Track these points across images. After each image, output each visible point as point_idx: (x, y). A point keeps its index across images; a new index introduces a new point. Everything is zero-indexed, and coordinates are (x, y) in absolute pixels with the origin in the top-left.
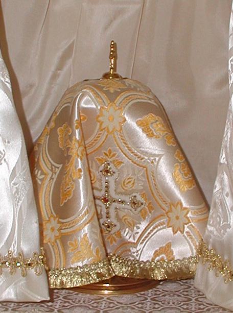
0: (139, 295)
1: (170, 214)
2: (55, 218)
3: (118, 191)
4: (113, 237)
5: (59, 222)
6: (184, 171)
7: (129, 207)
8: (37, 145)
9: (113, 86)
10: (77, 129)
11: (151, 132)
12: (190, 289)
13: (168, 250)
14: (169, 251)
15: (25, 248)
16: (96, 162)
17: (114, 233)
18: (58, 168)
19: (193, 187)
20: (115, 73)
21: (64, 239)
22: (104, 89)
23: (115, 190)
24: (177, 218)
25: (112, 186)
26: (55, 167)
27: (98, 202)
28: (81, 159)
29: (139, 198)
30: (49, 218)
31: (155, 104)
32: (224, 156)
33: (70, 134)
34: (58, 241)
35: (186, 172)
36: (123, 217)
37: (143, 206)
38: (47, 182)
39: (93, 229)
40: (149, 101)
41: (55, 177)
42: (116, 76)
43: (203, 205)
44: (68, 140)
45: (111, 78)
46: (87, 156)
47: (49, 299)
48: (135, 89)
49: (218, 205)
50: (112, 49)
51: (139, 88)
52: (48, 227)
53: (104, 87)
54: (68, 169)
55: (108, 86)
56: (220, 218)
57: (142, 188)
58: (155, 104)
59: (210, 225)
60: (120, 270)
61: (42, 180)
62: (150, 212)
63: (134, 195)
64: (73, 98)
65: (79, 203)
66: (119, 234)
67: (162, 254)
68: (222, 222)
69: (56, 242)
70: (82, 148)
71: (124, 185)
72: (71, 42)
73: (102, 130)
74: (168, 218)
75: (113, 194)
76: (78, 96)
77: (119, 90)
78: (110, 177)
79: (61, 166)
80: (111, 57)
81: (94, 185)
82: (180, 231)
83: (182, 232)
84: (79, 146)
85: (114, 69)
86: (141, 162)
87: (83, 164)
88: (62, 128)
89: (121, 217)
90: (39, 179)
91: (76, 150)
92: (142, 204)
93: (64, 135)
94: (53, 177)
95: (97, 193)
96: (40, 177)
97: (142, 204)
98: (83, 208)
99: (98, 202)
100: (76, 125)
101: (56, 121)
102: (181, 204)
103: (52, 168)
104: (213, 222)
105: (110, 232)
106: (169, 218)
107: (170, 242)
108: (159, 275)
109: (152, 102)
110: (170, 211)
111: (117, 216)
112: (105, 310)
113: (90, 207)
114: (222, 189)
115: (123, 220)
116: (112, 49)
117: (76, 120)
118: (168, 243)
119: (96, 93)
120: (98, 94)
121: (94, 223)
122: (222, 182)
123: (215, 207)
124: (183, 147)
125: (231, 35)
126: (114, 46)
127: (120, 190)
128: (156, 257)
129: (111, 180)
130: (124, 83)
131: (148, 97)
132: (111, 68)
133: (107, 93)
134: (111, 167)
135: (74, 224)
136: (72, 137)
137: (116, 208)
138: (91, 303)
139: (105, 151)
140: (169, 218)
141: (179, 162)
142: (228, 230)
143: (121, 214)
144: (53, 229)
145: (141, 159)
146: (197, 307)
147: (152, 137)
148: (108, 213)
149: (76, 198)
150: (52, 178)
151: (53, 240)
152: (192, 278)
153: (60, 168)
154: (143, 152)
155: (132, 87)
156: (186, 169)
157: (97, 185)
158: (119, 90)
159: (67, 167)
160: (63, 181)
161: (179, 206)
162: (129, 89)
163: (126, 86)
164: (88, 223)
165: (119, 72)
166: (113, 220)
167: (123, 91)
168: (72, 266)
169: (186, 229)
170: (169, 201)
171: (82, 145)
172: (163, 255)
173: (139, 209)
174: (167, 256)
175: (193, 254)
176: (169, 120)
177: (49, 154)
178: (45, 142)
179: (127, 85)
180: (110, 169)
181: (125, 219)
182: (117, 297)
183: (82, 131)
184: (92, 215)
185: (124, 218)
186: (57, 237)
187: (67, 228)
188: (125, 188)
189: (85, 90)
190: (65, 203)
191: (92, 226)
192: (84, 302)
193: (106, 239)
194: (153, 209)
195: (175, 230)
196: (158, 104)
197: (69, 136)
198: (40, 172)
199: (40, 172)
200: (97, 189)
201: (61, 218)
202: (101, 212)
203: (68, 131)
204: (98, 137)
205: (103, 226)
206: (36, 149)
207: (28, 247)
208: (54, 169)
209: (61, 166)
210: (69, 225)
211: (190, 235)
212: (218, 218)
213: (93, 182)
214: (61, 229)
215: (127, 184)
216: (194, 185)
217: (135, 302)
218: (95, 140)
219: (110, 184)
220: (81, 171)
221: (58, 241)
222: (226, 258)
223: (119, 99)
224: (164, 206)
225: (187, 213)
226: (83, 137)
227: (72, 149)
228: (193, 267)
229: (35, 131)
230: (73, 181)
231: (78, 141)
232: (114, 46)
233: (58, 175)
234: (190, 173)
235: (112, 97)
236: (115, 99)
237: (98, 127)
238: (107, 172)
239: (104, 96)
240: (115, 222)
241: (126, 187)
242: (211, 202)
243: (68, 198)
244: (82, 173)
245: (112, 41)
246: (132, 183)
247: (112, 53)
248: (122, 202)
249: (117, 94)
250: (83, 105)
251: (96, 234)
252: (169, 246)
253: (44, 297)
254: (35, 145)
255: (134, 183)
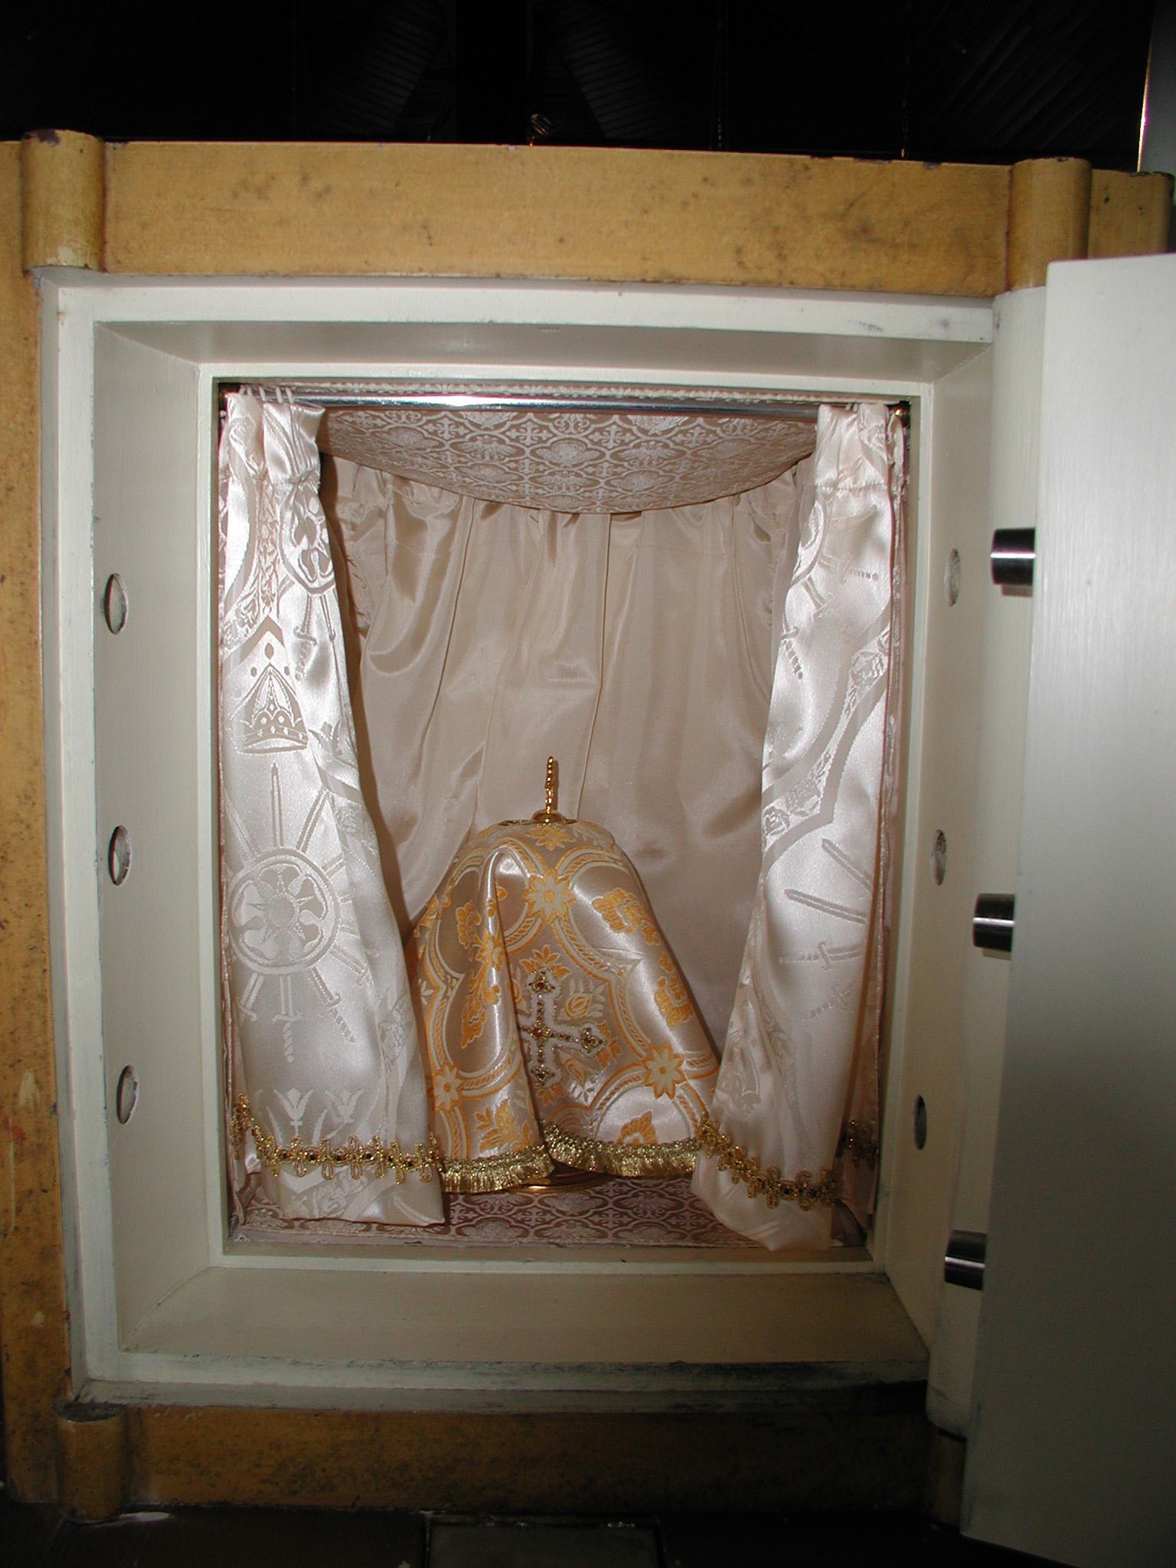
0: (593, 1194)
1: (650, 1064)
2: (452, 1068)
3: (559, 1018)
4: (549, 1092)
5: (458, 1076)
6: (674, 990)
7: (579, 1047)
8: (418, 928)
9: (554, 835)
10: (491, 915)
11: (617, 921)
12: (443, 449)
13: (646, 1126)
14: (648, 1128)
15: (405, 1137)
16: (521, 968)
17: (552, 1086)
18: (457, 979)
19: (690, 1016)
20: (554, 812)
21: (467, 1106)
22: (537, 844)
23: (555, 1020)
24: (663, 1071)
25: (550, 1009)
26: (453, 977)
27: (524, 1034)
28: (498, 969)
29: (596, 1032)
30: (441, 1066)
31: (622, 869)
32: (748, 973)
33: (478, 924)
34: (456, 1108)
35: (678, 991)
36: (567, 1061)
37: (602, 1046)
38: (437, 1003)
39: (518, 1092)
40: (614, 865)
41: (452, 994)
42: (556, 818)
43: (708, 1050)
44: (476, 935)
45: (547, 821)
46: (508, 961)
47: (443, 1221)
48: (589, 843)
49: (737, 1058)
50: (550, 772)
51: (597, 839)
52: (440, 1081)
53: (536, 840)
54: (476, 986)
55: (542, 838)
56: (740, 1082)
57: (601, 1014)
58: (622, 869)
59: (722, 1090)
60: (565, 1153)
61: (430, 998)
62: (615, 1056)
63: (587, 1026)
64: (484, 859)
65: (493, 1052)
66: (560, 1088)
67: (635, 1131)
68: (744, 1089)
69: (454, 1111)
70: (499, 949)
71: (570, 1008)
72: (477, 750)
73: (533, 915)
74: (645, 1071)
75: (551, 1026)
76: (491, 857)
77: (563, 847)
78: (546, 995)
79: (462, 977)
80: (549, 785)
81: (518, 1007)
82: (667, 1093)
83: (671, 1096)
84: (495, 947)
85: (554, 805)
86: (600, 973)
87: (501, 979)
88: (464, 909)
89: (563, 1062)
90: (425, 997)
91: (490, 953)
92: (601, 1042)
93: (467, 923)
94: (449, 994)
95: (524, 1021)
96: (425, 992)
97: (601, 1042)
98: (500, 1057)
99: (524, 1034)
100: (488, 908)
101: (451, 895)
102: (670, 1048)
103: (447, 979)
104: (727, 1085)
105: (543, 1085)
106: (648, 1069)
107: (650, 1113)
108: (629, 1167)
109: (620, 867)
110: (650, 1058)
111: (557, 1060)
112: (537, 1228)
113: (512, 1053)
114: (746, 1031)
115: (567, 1066)
116: (550, 772)
117: (490, 901)
118: (647, 1113)
119: (522, 853)
120: (527, 853)
121: (520, 1081)
122: (744, 1017)
123: (731, 1058)
124: (663, 928)
125: (767, 766)
126: (553, 767)
127: (563, 1016)
128: (624, 1136)
129: (548, 999)
130: (570, 833)
131: (612, 858)
132: (548, 805)
133: (542, 851)
134: (549, 979)
135: (485, 1083)
136: (483, 929)
137: (556, 1047)
138: (513, 1212)
139: (537, 951)
140: (648, 1069)
141: (665, 975)
142: (755, 1105)
143: (564, 1056)
144: (447, 1088)
145: (601, 967)
146: (443, 457)
147: (620, 929)
148: (541, 1055)
149: (488, 1038)
150: (445, 996)
151: (448, 1107)
152: (689, 1175)
153: (461, 980)
154: (604, 954)
155: (585, 839)
156: (677, 986)
157: (522, 1006)
158: (563, 847)
159: (472, 982)
160: (467, 1005)
161: (666, 1051)
162: (579, 844)
163: (574, 837)
164: (509, 1081)
165: (561, 810)
166: (549, 1065)
167: (570, 847)
168: (482, 1156)
169: (679, 1092)
170: (649, 1042)
171: (500, 945)
172: (637, 1135)
173: (595, 1051)
174: (645, 1136)
175: (689, 1133)
176: (645, 891)
177: (442, 954)
178: (430, 921)
179: (576, 835)
180: (546, 982)
181: (570, 1066)
182: (556, 1198)
183: (500, 919)
184: (517, 1066)
185: (570, 1063)
186: (456, 1102)
187: (473, 1089)
188: (572, 1015)
189: (504, 846)
190: (469, 1044)
191: (517, 1086)
192: (500, 1209)
193: (537, 1095)
194: (618, 1052)
195: (659, 1092)
196: (629, 871)
197: (477, 927)
198: (425, 983)
199: (425, 983)
200: (523, 1013)
201: (463, 1070)
202: (529, 1052)
203: (477, 919)
204: (526, 927)
205: (532, 1075)
206: (417, 933)
207: (413, 1135)
208: (449, 981)
209: (462, 977)
210: (477, 1084)
211: (685, 1103)
212: (737, 1082)
213: (517, 1001)
214: (463, 1089)
215: (575, 1007)
216: (691, 1014)
217: (588, 1211)
218: (521, 932)
219: (545, 1015)
220: (498, 991)
221: (456, 1108)
222: (751, 1154)
223: (564, 862)
224: (639, 1049)
225: (680, 1064)
226: (501, 927)
227: (482, 951)
228: (691, 1159)
229: (414, 895)
230: (484, 1007)
231: (493, 937)
232: (553, 767)
233: (457, 992)
234: (685, 992)
235: (550, 859)
236: (556, 862)
237: (526, 909)
238: (541, 986)
239: (536, 858)
240: (552, 1068)
241: (573, 1012)
242: (723, 1050)
243: (475, 1036)
244: (499, 994)
245: (551, 758)
246: (585, 1004)
247: (549, 779)
248: (568, 1038)
249: (560, 852)
250: (502, 870)
251: (523, 1100)
252: (648, 1118)
253: (434, 1218)
254: (414, 928)
255: (586, 1007)
